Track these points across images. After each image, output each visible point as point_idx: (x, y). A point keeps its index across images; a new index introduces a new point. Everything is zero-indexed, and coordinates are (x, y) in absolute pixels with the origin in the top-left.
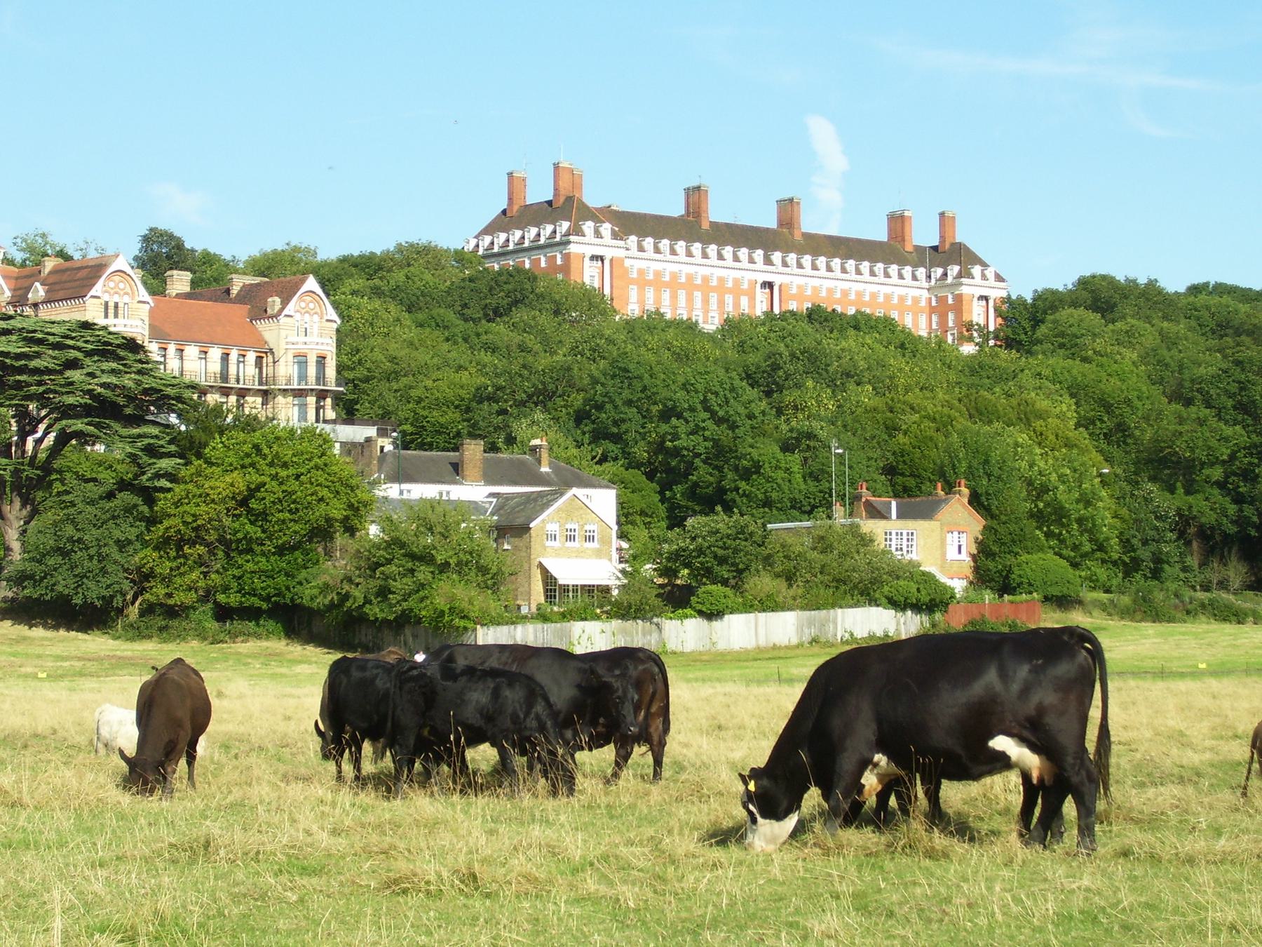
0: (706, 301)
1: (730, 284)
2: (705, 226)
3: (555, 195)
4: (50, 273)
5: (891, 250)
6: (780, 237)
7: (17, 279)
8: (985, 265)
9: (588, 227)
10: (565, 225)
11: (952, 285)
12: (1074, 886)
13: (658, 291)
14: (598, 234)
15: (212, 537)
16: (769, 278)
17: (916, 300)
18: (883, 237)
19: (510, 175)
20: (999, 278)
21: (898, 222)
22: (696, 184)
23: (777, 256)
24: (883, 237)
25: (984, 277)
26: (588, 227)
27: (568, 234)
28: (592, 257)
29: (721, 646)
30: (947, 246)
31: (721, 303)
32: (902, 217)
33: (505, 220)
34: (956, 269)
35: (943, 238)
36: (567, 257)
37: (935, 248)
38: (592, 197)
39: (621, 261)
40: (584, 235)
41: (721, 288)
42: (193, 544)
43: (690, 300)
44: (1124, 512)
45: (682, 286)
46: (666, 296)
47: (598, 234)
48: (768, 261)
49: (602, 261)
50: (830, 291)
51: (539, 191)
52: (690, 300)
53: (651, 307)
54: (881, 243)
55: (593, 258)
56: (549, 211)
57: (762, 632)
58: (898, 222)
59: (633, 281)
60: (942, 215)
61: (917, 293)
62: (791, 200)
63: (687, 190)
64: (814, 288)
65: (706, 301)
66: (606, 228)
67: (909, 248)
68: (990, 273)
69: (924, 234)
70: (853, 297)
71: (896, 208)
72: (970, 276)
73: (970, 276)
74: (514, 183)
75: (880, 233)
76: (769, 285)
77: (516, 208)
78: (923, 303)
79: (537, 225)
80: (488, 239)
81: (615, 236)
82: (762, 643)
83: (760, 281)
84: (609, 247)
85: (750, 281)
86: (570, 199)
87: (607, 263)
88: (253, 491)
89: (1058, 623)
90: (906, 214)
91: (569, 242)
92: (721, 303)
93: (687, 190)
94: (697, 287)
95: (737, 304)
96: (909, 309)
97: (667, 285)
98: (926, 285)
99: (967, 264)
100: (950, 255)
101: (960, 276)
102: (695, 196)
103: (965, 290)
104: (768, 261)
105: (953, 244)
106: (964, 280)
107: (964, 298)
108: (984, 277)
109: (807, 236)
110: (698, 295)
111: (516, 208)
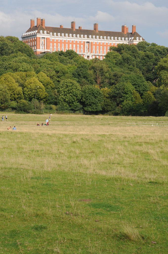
3: (37, 24)
8: (140, 36)
9: (41, 31)
10: (133, 38)
12: (13, 144)
16: (88, 41)
18: (70, 27)
19: (31, 20)
24: (70, 27)
27: (133, 40)
36: (36, 38)
37: (131, 33)
39: (49, 38)
40: (136, 40)
43: (72, 46)
50: (114, 44)
52: (72, 46)
53: (70, 49)
54: (69, 29)
55: (42, 38)
56: (36, 28)
59: (51, 42)
62: (96, 24)
63: (94, 24)
64: (57, 40)
66: (45, 32)
74: (32, 21)
81: (47, 33)
84: (46, 36)
90: (125, 26)
91: (133, 41)
93: (94, 24)
94: (101, 45)
97: (63, 43)
98: (128, 41)
99: (136, 37)
100: (134, 34)
104: (88, 37)
108: (139, 39)
111: (32, 27)
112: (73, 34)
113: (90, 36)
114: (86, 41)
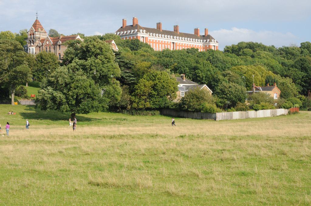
0: (156, 45)
1: (166, 43)
2: (161, 31)
4: (61, 39)
5: (195, 35)
6: (175, 33)
7: (53, 40)
8: (214, 39)
9: (141, 30)
11: (135, 34)
13: (179, 47)
14: (143, 32)
15: (147, 94)
17: (201, 46)
20: (217, 42)
21: (196, 31)
22: (159, 22)
23: (175, 37)
24: (156, 28)
25: (214, 42)
26: (141, 30)
27: (137, 32)
28: (142, 36)
29: (258, 117)
30: (206, 35)
31: (162, 46)
32: (197, 29)
33: (122, 29)
34: (136, 30)
35: (205, 34)
38: (141, 24)
39: (147, 37)
41: (162, 43)
42: (143, 96)
44: (138, 93)
45: (157, 43)
46: (169, 46)
47: (143, 32)
48: (173, 38)
49: (144, 38)
51: (129, 23)
55: (142, 37)
57: (265, 115)
58: (196, 31)
60: (205, 29)
61: (201, 45)
65: (156, 45)
66: (144, 31)
67: (199, 36)
68: (215, 41)
69: (202, 33)
70: (163, 42)
71: (196, 27)
72: (212, 41)
73: (212, 41)
75: (172, 30)
76: (173, 43)
77: (124, 26)
78: (202, 47)
79: (130, 30)
80: (119, 33)
81: (146, 33)
82: (265, 116)
83: (172, 42)
84: (146, 35)
85: (155, 40)
86: (137, 25)
87: (215, 47)
88: (155, 85)
89: (307, 113)
91: (137, 34)
92: (162, 46)
95: (165, 46)
96: (151, 42)
98: (202, 43)
100: (206, 37)
101: (210, 41)
102: (159, 25)
103: (211, 44)
104: (173, 38)
105: (208, 35)
106: (138, 33)
107: (211, 46)
108: (214, 42)
109: (180, 33)
110: (160, 45)
111: (124, 26)
112: (198, 39)
113: (175, 37)
114: (172, 41)
